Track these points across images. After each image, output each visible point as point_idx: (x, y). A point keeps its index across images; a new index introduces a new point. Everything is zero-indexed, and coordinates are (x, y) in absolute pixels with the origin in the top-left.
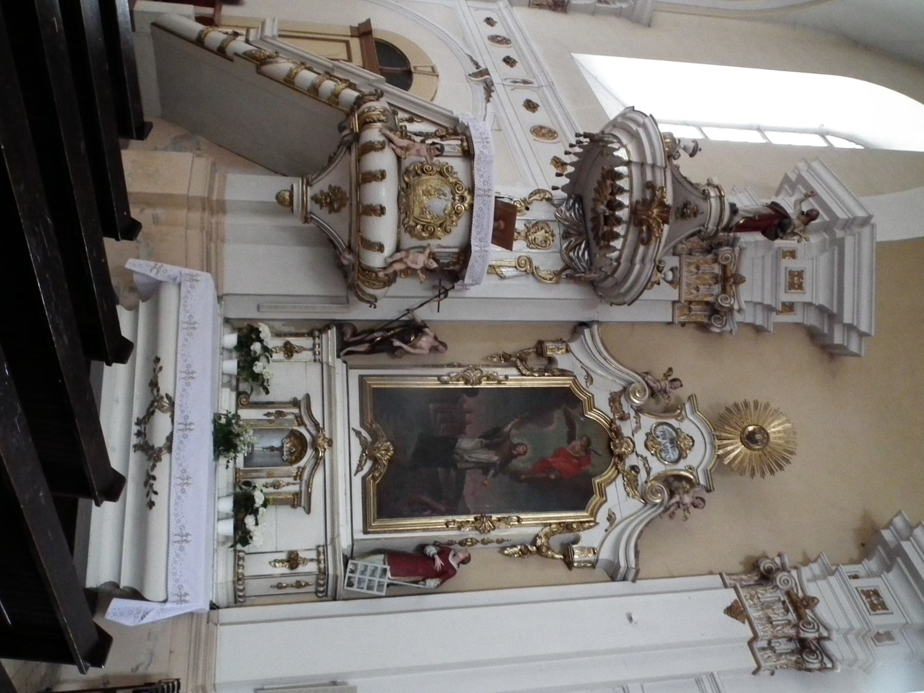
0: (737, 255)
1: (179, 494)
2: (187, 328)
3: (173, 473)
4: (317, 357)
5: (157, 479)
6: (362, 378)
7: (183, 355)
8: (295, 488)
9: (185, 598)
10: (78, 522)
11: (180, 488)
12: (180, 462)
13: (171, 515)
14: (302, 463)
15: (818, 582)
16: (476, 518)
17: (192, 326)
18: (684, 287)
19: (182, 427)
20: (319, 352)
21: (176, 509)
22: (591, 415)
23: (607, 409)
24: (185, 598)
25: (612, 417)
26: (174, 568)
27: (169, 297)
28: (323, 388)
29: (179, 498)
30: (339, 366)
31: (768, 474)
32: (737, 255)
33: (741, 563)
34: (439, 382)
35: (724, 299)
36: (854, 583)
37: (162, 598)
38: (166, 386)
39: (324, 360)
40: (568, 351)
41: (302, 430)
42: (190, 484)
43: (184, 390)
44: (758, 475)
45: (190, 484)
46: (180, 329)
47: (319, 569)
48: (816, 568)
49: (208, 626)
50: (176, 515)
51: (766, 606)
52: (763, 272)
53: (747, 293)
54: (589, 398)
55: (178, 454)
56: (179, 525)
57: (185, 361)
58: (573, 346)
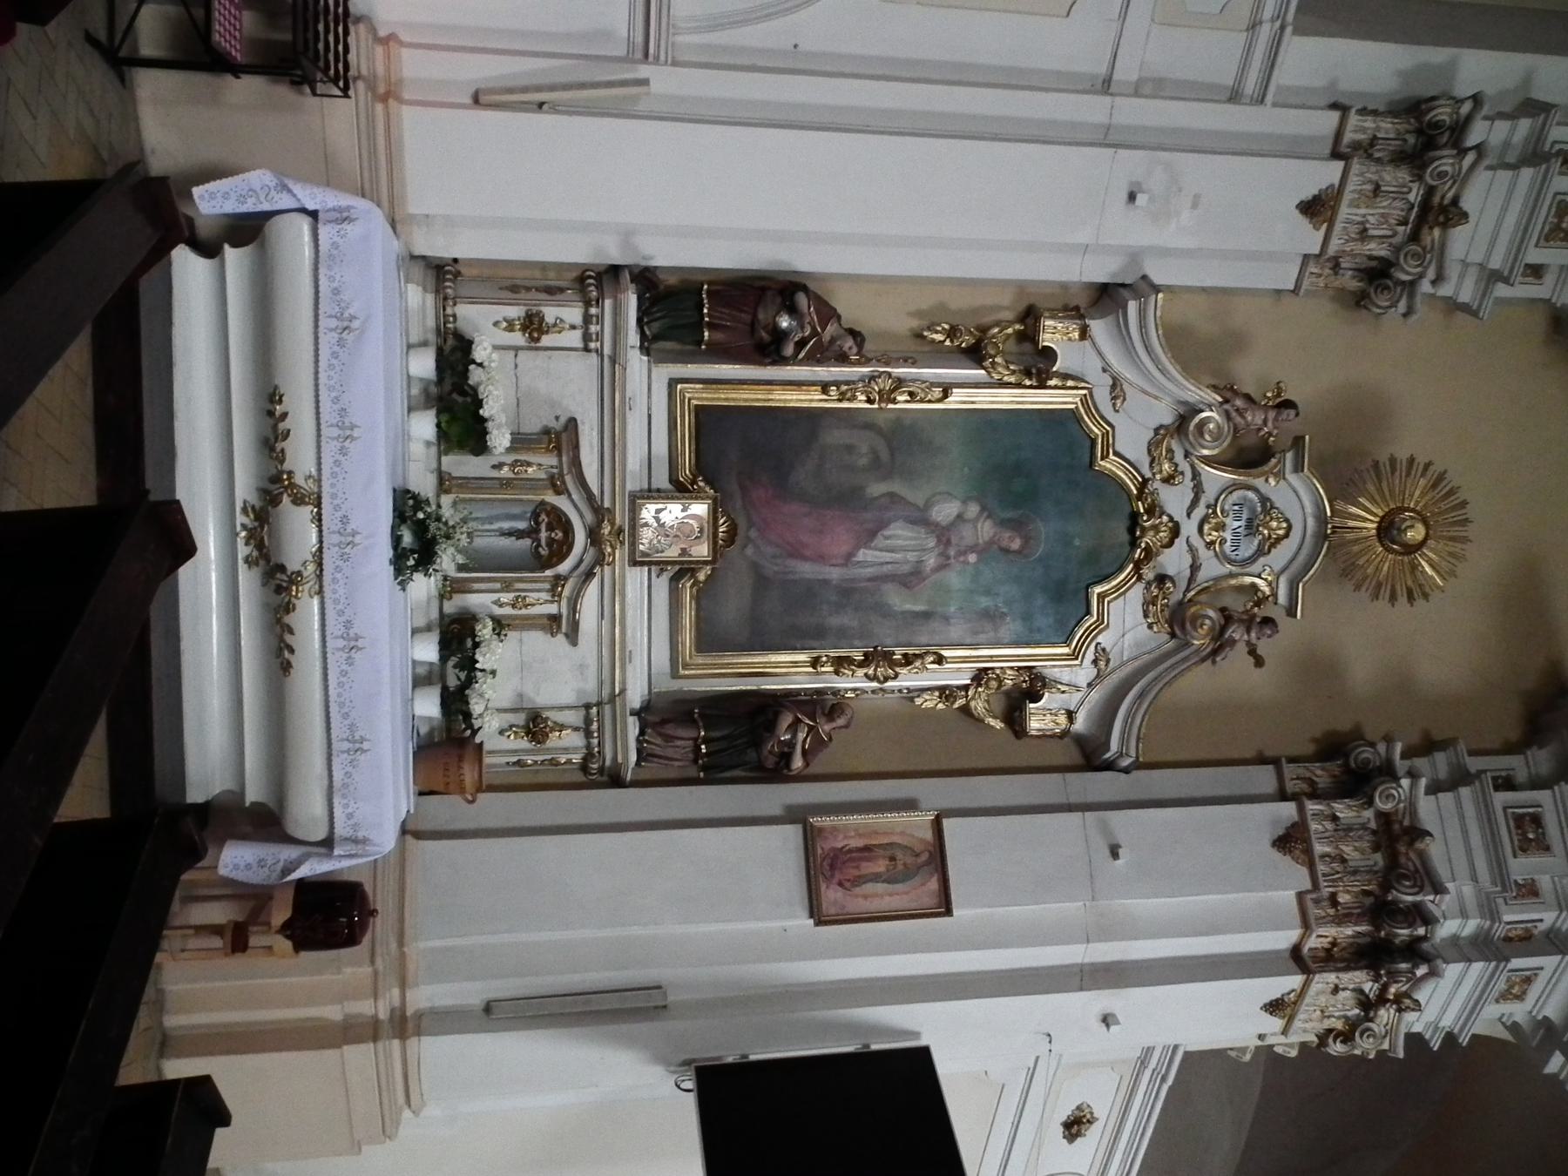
0: (1464, 170)
1: (344, 667)
2: (348, 751)
3: (324, 417)
4: (592, 345)
5: (296, 652)
6: (673, 383)
7: (334, 496)
8: (552, 609)
9: (361, 746)
10: (146, 383)
11: (339, 445)
12: (340, 607)
13: (321, 387)
14: (564, 567)
15: (1440, 795)
16: (866, 654)
17: (358, 745)
18: (1338, 226)
19: (346, 745)
20: (597, 334)
21: (333, 485)
22: (1110, 465)
23: (1140, 455)
24: (361, 746)
25: (1148, 475)
26: (339, 695)
27: (294, 237)
28: (602, 466)
29: (344, 673)
30: (636, 361)
31: (1403, 600)
32: (1464, 170)
33: (1315, 740)
34: (816, 821)
35: (1413, 256)
36: (1501, 798)
37: (321, 834)
38: (300, 459)
39: (607, 351)
40: (1084, 333)
41: (562, 502)
42: (356, 439)
43: (337, 463)
44: (1385, 593)
45: (356, 439)
46: (321, 329)
47: (589, 746)
48: (1441, 763)
49: (404, 841)
50: (341, 705)
51: (1344, 831)
52: (1505, 209)
53: (1462, 243)
54: (1105, 435)
55: (335, 591)
56: (346, 722)
57: (346, 716)
58: (1097, 327)
